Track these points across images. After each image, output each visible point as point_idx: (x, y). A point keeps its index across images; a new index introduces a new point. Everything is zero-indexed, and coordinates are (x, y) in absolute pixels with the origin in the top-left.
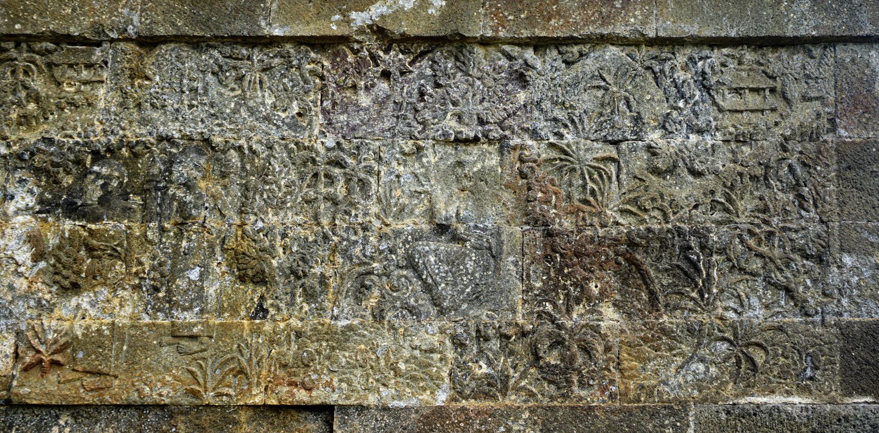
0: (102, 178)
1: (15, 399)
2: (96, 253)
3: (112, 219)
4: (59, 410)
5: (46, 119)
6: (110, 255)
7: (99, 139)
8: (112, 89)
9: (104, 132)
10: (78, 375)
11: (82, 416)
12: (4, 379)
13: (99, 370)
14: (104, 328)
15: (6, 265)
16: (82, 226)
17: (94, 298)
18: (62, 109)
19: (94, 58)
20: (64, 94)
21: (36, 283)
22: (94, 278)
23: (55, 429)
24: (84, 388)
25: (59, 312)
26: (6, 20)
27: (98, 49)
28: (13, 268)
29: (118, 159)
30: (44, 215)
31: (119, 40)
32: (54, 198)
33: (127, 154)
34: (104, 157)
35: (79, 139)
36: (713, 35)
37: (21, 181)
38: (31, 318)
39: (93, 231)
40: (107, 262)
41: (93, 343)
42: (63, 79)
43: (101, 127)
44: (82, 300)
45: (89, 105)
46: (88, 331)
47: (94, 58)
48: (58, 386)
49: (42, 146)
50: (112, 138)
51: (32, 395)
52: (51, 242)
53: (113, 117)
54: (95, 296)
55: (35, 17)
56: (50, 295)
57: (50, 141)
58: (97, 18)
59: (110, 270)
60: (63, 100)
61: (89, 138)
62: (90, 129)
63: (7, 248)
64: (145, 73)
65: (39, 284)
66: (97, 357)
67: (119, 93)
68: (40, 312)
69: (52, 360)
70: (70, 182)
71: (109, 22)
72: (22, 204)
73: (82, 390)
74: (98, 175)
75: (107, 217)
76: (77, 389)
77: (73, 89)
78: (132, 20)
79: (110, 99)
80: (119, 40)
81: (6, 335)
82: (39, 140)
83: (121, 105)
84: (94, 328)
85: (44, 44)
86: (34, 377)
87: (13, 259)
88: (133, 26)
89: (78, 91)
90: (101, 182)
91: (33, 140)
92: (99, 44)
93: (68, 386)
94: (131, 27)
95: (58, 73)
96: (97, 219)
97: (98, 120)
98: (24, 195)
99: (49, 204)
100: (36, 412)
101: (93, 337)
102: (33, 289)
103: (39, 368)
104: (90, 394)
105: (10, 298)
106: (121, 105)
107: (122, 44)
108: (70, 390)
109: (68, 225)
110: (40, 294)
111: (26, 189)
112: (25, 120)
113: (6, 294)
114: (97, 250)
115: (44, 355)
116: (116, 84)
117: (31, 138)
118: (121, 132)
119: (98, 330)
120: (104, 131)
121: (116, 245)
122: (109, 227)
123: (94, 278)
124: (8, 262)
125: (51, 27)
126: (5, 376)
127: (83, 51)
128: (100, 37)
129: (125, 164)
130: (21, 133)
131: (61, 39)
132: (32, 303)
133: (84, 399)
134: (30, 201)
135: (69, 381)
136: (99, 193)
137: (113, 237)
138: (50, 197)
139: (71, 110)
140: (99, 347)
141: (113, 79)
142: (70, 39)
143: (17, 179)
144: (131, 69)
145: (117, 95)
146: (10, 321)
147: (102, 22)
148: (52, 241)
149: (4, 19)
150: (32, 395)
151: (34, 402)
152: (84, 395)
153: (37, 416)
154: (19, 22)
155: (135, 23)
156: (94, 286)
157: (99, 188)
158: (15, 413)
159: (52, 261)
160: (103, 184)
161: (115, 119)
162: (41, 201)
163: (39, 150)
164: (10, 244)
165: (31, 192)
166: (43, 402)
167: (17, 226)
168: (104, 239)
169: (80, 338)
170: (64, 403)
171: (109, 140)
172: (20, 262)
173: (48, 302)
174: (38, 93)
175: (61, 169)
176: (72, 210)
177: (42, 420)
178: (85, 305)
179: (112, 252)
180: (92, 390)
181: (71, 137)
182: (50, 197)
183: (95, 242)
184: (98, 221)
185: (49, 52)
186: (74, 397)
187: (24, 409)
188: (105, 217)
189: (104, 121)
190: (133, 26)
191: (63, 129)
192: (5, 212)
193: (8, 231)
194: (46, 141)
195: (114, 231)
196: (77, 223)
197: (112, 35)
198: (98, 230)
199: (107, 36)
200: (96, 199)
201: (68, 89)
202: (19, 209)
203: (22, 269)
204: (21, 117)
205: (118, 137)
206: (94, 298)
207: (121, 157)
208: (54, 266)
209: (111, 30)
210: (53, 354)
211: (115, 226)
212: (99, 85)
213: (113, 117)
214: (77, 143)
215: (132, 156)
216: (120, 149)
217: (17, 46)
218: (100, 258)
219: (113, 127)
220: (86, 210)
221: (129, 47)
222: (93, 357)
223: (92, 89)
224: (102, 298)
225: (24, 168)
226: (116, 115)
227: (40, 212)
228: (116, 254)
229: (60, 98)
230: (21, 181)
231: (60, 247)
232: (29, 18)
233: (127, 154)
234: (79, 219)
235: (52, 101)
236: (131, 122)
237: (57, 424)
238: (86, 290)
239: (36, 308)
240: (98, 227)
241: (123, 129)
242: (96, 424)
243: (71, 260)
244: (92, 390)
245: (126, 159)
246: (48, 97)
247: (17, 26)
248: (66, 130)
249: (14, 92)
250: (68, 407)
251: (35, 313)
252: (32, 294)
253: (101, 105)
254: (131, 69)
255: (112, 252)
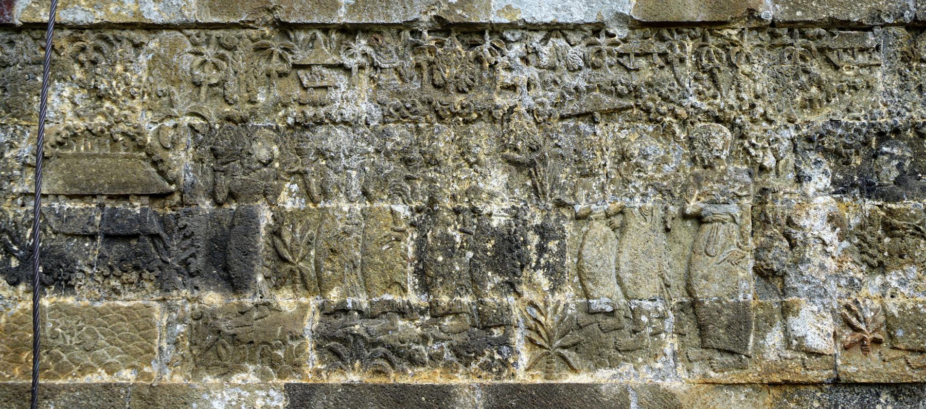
0: (896, 159)
1: (843, 378)
2: (897, 232)
3: (913, 198)
4: (879, 388)
5: (828, 101)
6: (912, 234)
7: (885, 121)
8: (887, 72)
9: (890, 114)
10: (900, 353)
11: (904, 394)
12: (830, 357)
13: (922, 348)
14: (920, 306)
15: (813, 245)
16: (879, 206)
17: (904, 277)
18: (843, 92)
19: (869, 43)
20: (844, 78)
21: (846, 262)
22: (901, 257)
23: (878, 407)
24: (910, 366)
25: (866, 291)
26: (787, 8)
27: (870, 33)
28: (819, 247)
29: (903, 140)
30: (838, 196)
31: (893, 25)
32: (845, 178)
33: (911, 135)
34: (889, 138)
35: (865, 121)
36: (94, 22)
37: (817, 162)
38: (840, 297)
39: (894, 210)
40: (911, 241)
41: (912, 321)
42: (841, 63)
43: (886, 109)
44: (891, 278)
45: (868, 87)
46: (904, 309)
47: (869, 43)
48: (884, 365)
49: (830, 127)
50: (897, 119)
51: (861, 374)
52: (852, 221)
53: (897, 100)
54: (905, 274)
55: (814, 5)
56: (861, 274)
57: (837, 123)
58: (874, 4)
59: (916, 248)
60: (844, 84)
61: (875, 120)
62: (875, 111)
63: (813, 228)
64: (921, 56)
65: (849, 263)
66: (918, 335)
67: (898, 76)
68: (849, 291)
69: (874, 338)
70: (859, 162)
71: (886, 7)
72: (821, 186)
73: (908, 368)
74: (892, 156)
75: (907, 196)
76: (903, 367)
77: (851, 73)
78: (908, 5)
79: (889, 82)
80: (893, 25)
81: (825, 314)
82: (827, 123)
83: (901, 87)
84: (910, 306)
85: (817, 30)
86: (856, 355)
87: (820, 238)
88: (910, 11)
89: (857, 75)
90: (895, 163)
91: (821, 123)
92: (870, 29)
93: (893, 364)
94: (908, 12)
95: (834, 58)
96: (898, 199)
97: (882, 102)
98: (821, 176)
99: (842, 185)
100: (856, 391)
101: (910, 315)
102: (844, 269)
103: (859, 347)
104: (916, 372)
105: (823, 278)
106: (901, 87)
107: (893, 28)
108: (896, 368)
109: (869, 205)
110: (852, 274)
111: (821, 170)
112: (810, 104)
113: (818, 274)
114: (899, 229)
115: (866, 334)
116: (890, 67)
117: (819, 119)
118: (907, 114)
119: (914, 308)
120: (890, 113)
121: (919, 224)
122: (910, 206)
123: (901, 257)
124: (815, 242)
125: (831, 13)
126: (830, 355)
127: (856, 36)
128: (873, 22)
129: (910, 144)
130: (806, 116)
131: (836, 25)
132: (843, 282)
133: (912, 377)
134: (826, 182)
135: (893, 359)
136: (895, 174)
137: (914, 217)
138: (841, 177)
139: (850, 93)
140: (919, 325)
141: (887, 63)
142: (846, 25)
143: (813, 161)
144: (902, 53)
145: (896, 77)
146: (825, 300)
147: (880, 8)
148: (854, 221)
149: (785, 6)
150: (861, 374)
151: (863, 381)
152: (910, 373)
153: (858, 394)
154: (799, 10)
155: (912, 9)
156: (901, 265)
157: (895, 168)
158: (837, 392)
159: (857, 241)
160: (898, 164)
161: (899, 101)
162: (833, 183)
163: (829, 132)
164: (815, 224)
165: (825, 172)
166: (872, 380)
167: (820, 206)
168: (905, 218)
169: (897, 316)
170: (892, 381)
171: (896, 122)
172: (828, 242)
173: (860, 281)
174: (820, 77)
175: (853, 150)
176: (870, 190)
177: (863, 398)
178: (894, 284)
179: (915, 231)
180: (918, 368)
181: (858, 119)
182: (841, 177)
183: (895, 221)
184: (898, 201)
185: (819, 36)
186: (902, 375)
187: (845, 388)
188: (905, 196)
189: (889, 103)
190: (910, 11)
191: (848, 111)
192: (804, 193)
193: (812, 211)
194: (833, 123)
195: (916, 211)
196: (876, 203)
197: (887, 20)
198: (899, 209)
199: (882, 21)
200: (893, 179)
201: (847, 73)
202: (819, 191)
203: (829, 249)
204: (806, 100)
205: (904, 118)
206: (904, 277)
207: (907, 138)
208: (859, 245)
209: (888, 16)
210: (874, 332)
211: (916, 206)
212: (876, 68)
213: (897, 100)
214: (864, 124)
215: (917, 137)
216: (906, 130)
217: (791, 33)
218: (902, 237)
219: (899, 109)
220: (884, 190)
221: (901, 31)
222: (913, 334)
223: (871, 73)
224: (911, 276)
225: (812, 150)
226: (899, 97)
227: (834, 193)
228: (918, 233)
229: (841, 82)
230: (817, 162)
231: (861, 227)
232: (808, 5)
233: (911, 135)
234: (877, 199)
235: (834, 84)
236: (914, 104)
237: (879, 403)
238: (893, 269)
239: (846, 286)
240: (898, 206)
241: (909, 111)
242: (919, 401)
243: (875, 239)
244: (918, 368)
245: (910, 139)
246: (830, 81)
247: (799, 13)
248: (852, 112)
249: (796, 77)
250: (887, 385)
251: (844, 292)
252: (843, 273)
253: (881, 87)
254: (902, 53)
255: (915, 231)
